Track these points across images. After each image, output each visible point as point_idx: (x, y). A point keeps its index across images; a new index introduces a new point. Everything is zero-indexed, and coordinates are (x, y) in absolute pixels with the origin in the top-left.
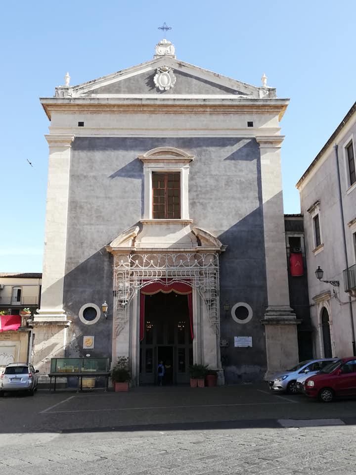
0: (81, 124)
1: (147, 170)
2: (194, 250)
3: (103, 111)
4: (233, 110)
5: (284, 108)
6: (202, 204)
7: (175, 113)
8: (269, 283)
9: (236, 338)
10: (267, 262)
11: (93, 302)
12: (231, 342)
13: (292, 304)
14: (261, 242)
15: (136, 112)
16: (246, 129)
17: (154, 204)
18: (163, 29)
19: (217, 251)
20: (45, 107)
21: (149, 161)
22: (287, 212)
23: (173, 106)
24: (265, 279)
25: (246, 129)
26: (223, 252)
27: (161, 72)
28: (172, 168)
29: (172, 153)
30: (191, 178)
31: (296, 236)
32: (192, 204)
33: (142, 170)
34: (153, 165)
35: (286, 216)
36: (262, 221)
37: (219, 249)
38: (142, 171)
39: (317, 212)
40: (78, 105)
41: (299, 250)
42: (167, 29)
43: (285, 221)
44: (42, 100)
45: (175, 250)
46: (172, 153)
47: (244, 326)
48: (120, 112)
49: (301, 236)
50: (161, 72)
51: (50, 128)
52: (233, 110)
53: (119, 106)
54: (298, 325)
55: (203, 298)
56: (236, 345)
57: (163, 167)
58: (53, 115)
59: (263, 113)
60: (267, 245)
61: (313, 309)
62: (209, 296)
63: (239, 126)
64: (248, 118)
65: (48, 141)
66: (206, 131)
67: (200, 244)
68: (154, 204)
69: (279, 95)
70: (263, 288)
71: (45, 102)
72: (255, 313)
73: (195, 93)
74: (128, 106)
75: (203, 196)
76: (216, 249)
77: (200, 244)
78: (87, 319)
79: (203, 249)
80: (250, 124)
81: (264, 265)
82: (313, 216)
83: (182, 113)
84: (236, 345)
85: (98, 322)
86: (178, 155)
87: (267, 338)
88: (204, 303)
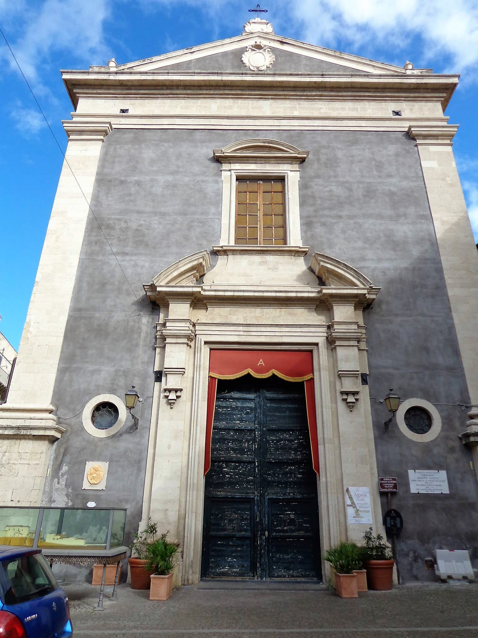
6: (324, 224)
9: (411, 472)
11: (113, 391)
24: (457, 353)
30: (304, 186)
47: (426, 448)
56: (414, 489)
75: (326, 212)
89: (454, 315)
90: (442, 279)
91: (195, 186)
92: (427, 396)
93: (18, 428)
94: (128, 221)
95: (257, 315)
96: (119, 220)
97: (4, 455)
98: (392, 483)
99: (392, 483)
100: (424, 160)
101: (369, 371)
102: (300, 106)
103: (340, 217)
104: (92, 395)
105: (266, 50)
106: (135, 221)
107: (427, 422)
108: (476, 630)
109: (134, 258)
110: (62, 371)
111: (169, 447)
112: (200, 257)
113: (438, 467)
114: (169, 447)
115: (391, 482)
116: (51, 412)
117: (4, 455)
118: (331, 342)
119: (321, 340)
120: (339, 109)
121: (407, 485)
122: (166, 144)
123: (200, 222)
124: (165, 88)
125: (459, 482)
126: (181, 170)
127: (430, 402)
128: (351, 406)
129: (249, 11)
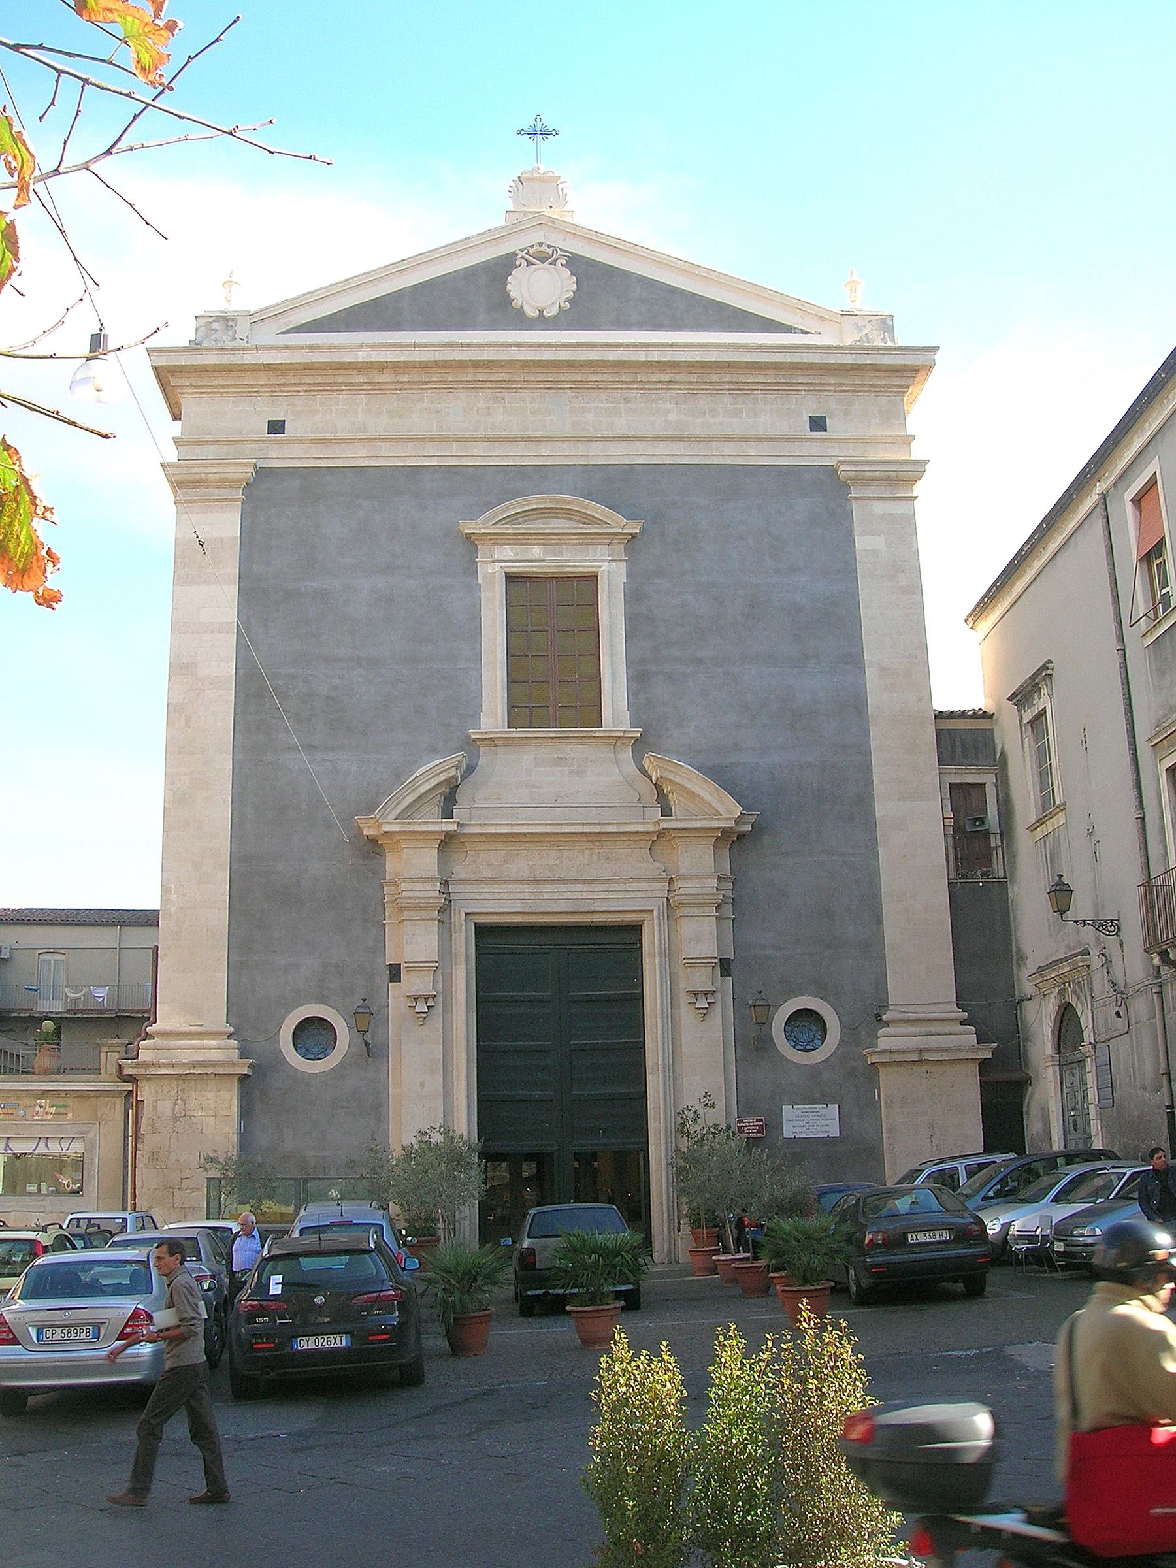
0: (276, 427)
1: (491, 568)
2: (650, 828)
3: (346, 384)
4: (760, 379)
5: (920, 377)
6: (670, 678)
7: (579, 387)
8: (891, 933)
9: (786, 1109)
10: (882, 864)
11: (322, 1000)
12: (774, 1124)
13: (962, 997)
14: (865, 800)
15: (450, 387)
16: (801, 440)
17: (482, 317)
18: (532, 133)
19: (725, 832)
20: (163, 375)
21: (497, 539)
22: (942, 703)
23: (570, 365)
24: (878, 920)
25: (801, 440)
26: (741, 836)
27: (529, 264)
28: (575, 561)
29: (569, 514)
30: (634, 596)
31: (970, 779)
32: (639, 677)
33: (471, 569)
34: (507, 552)
35: (940, 715)
36: (866, 732)
37: (732, 824)
38: (474, 574)
39: (1042, 702)
40: (268, 368)
41: (983, 823)
42: (546, 133)
43: (939, 732)
44: (154, 356)
45: (587, 829)
46: (569, 514)
47: (814, 1072)
48: (402, 387)
49: (989, 779)
50: (529, 264)
51: (177, 442)
52: (760, 379)
53: (397, 367)
54: (984, 1065)
55: (683, 985)
56: (788, 1132)
57: (543, 561)
58: (188, 404)
59: (855, 390)
60: (884, 809)
61: (1030, 1009)
62: (702, 979)
63: (783, 428)
64: (811, 406)
65: (171, 482)
66: (674, 444)
67: (666, 812)
68: (482, 317)
69: (905, 337)
70: (873, 948)
71: (163, 361)
72: (850, 1032)
73: (641, 326)
74: (425, 366)
75: (675, 652)
76: (723, 825)
77: (666, 812)
78: (794, 1043)
79: (679, 825)
80: (818, 424)
81: (873, 877)
82: (1028, 716)
83: (598, 387)
84: (788, 1132)
85: (342, 1064)
86: (589, 519)
87: (887, 1107)
88: (684, 999)
89: (881, 850)
90: (869, 782)
91: (429, 599)
92: (822, 991)
93: (194, 1065)
94: (310, 678)
95: (552, 862)
96: (293, 677)
97: (175, 1104)
98: (756, 1126)
99: (756, 1126)
100: (861, 534)
101: (208, 1313)
102: (629, 405)
103: (700, 661)
104: (290, 1007)
105: (558, 263)
106: (324, 678)
107: (818, 1035)
108: (1174, 1513)
109: (330, 756)
110: (234, 968)
111: (422, 1085)
112: (452, 765)
113: (825, 1099)
114: (422, 1085)
115: (755, 1124)
116: (230, 1036)
117: (175, 1104)
118: (671, 908)
119: (656, 905)
120: (705, 413)
121: (779, 1126)
122: (365, 503)
123: (443, 678)
124: (355, 372)
125: (854, 1120)
126: (399, 562)
127: (826, 1000)
128: (704, 1014)
129: (519, 132)
